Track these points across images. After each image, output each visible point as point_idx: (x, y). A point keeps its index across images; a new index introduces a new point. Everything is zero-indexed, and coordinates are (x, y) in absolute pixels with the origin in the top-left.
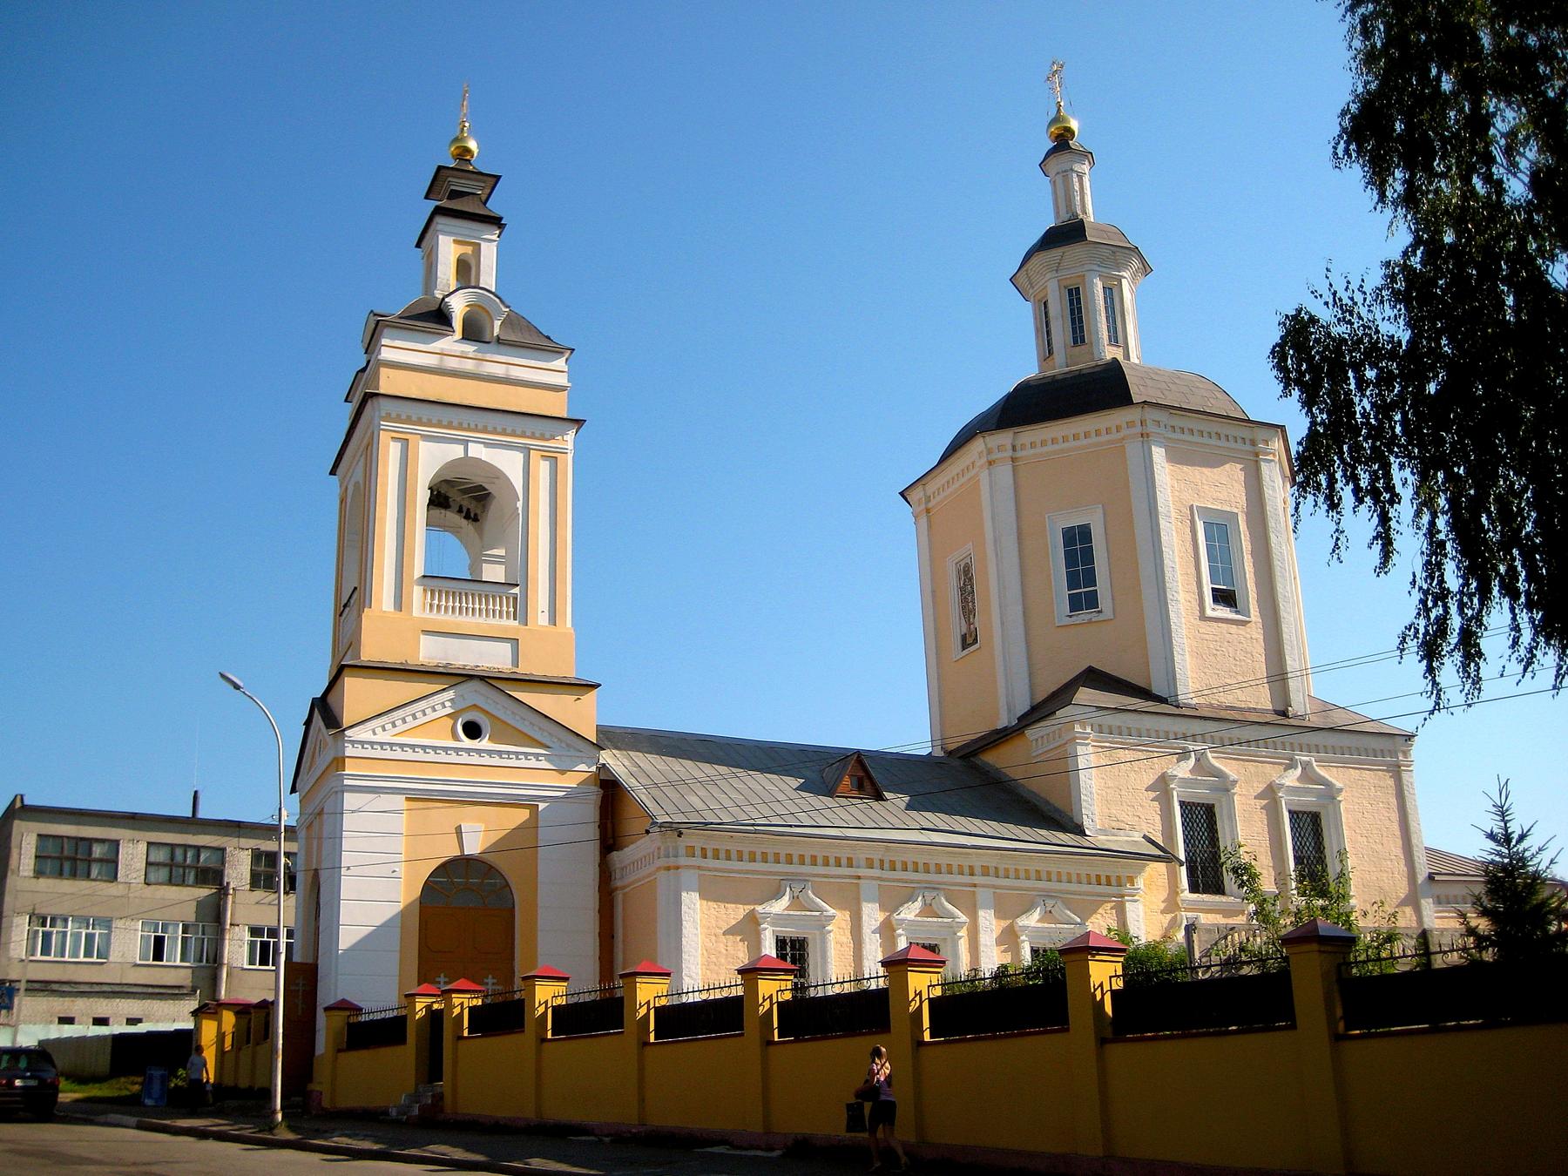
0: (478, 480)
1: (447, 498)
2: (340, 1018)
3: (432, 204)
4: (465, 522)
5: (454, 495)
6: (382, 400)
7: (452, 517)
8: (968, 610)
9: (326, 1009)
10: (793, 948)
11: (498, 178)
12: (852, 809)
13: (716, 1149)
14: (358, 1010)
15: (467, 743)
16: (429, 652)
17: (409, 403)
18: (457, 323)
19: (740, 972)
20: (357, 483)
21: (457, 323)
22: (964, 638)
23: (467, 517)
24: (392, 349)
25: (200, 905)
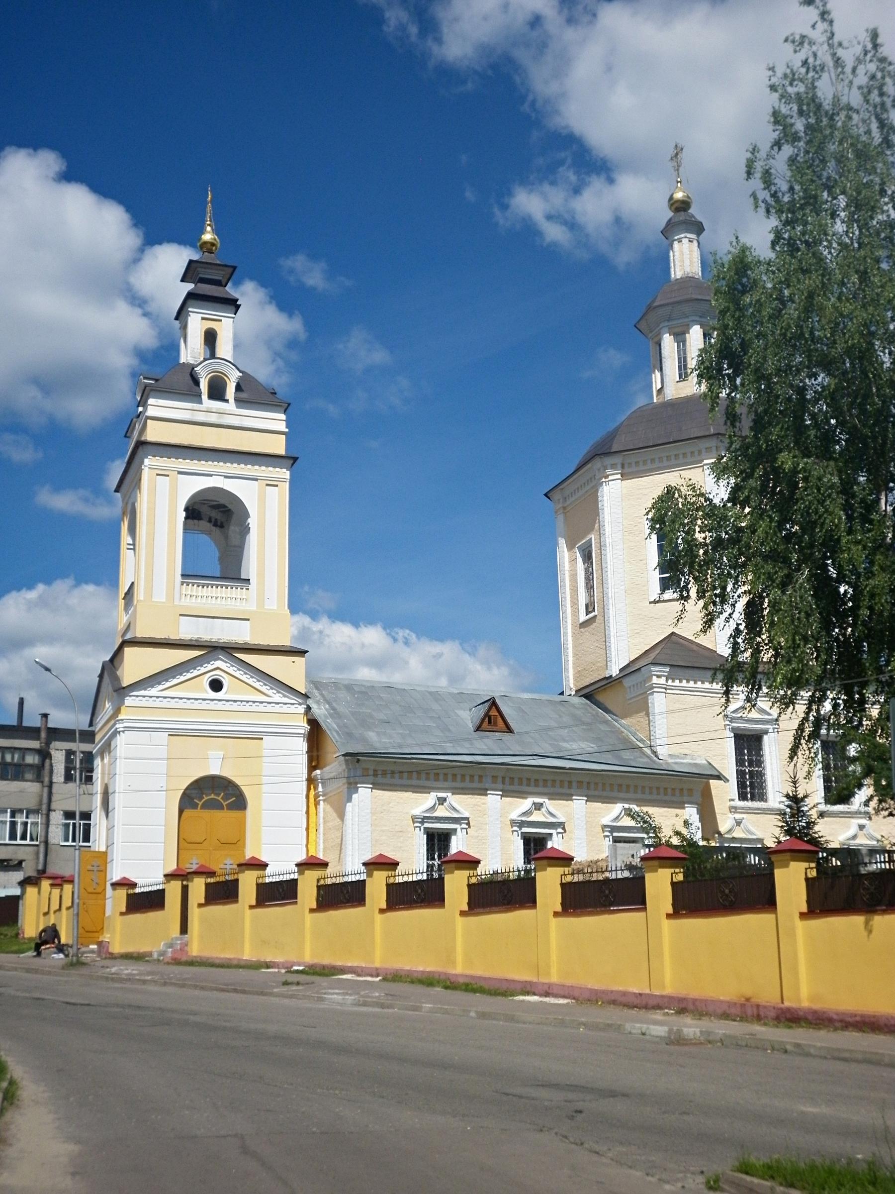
1: (199, 513)
2: (122, 893)
3: (189, 286)
4: (214, 528)
5: (205, 510)
6: (149, 447)
7: (204, 524)
8: (589, 587)
9: (113, 885)
10: (439, 840)
11: (234, 268)
12: (486, 740)
13: (344, 977)
14: (134, 885)
15: (213, 695)
16: (187, 630)
17: (168, 448)
19: (364, 864)
22: (587, 606)
23: (215, 525)
24: (156, 407)
25: (237, 284)
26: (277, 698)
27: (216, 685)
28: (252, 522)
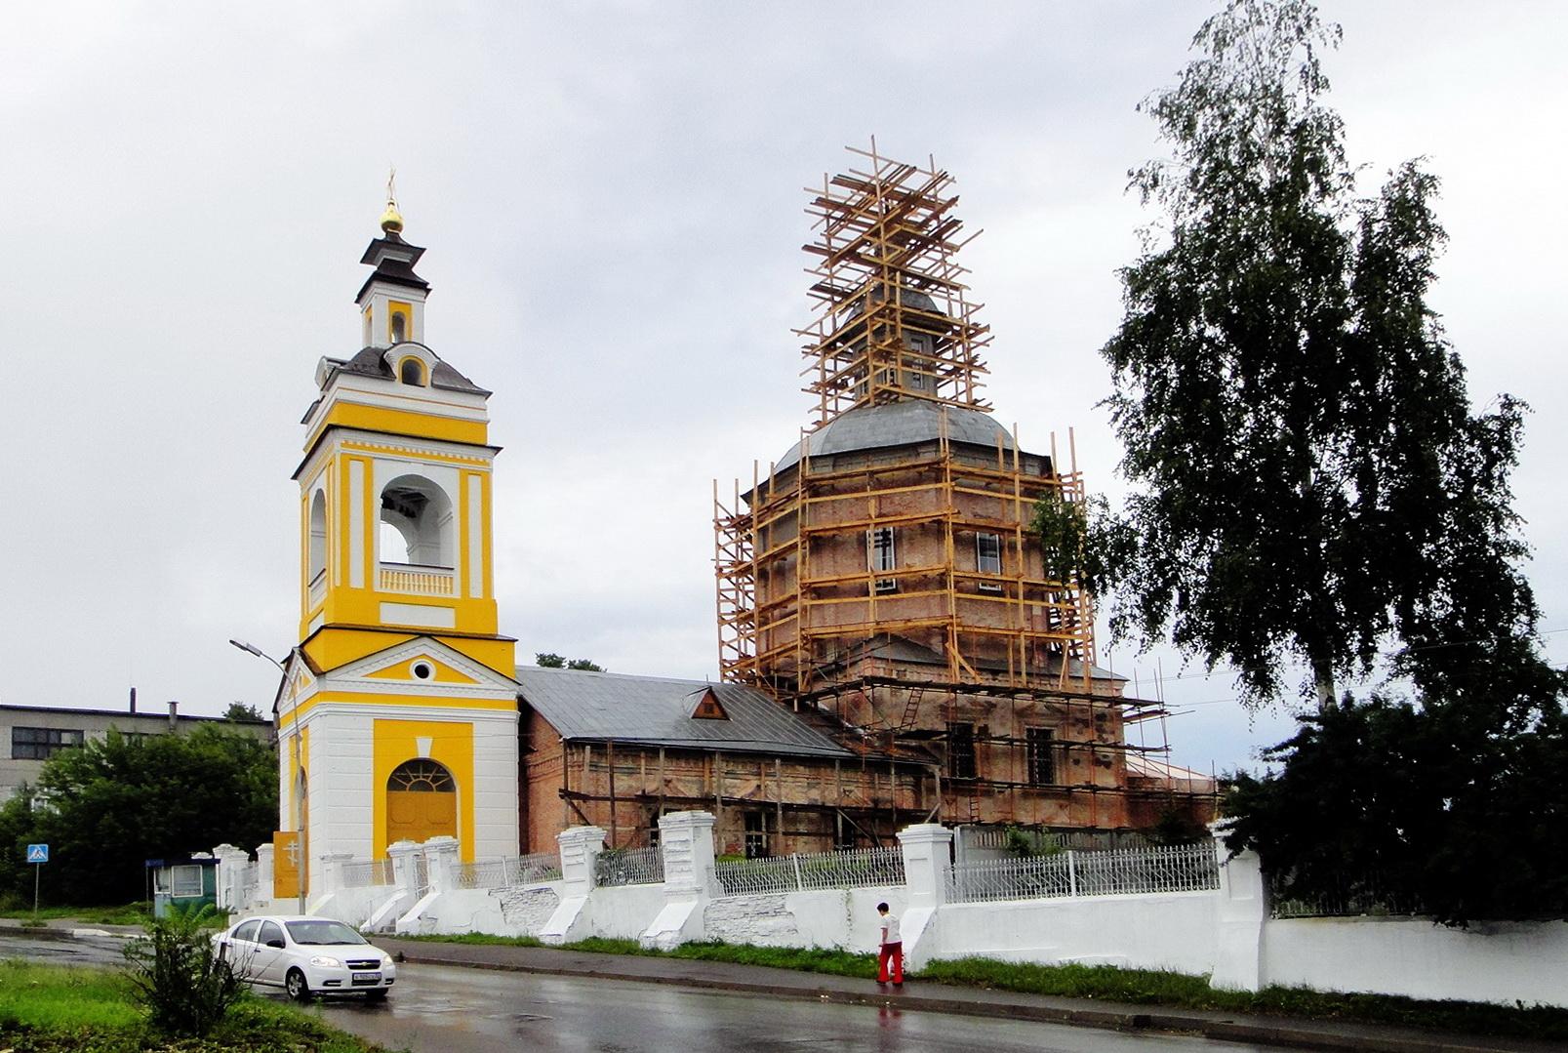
0: (416, 488)
6: (341, 432)
16: (390, 616)
18: (397, 370)
20: (320, 492)
21: (397, 370)
26: (486, 684)
27: (422, 672)
28: (455, 509)
